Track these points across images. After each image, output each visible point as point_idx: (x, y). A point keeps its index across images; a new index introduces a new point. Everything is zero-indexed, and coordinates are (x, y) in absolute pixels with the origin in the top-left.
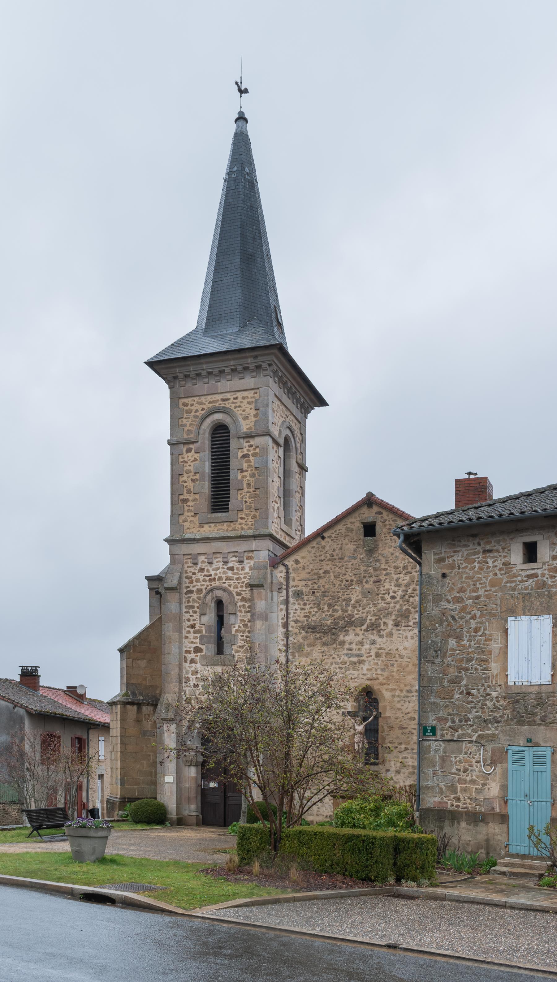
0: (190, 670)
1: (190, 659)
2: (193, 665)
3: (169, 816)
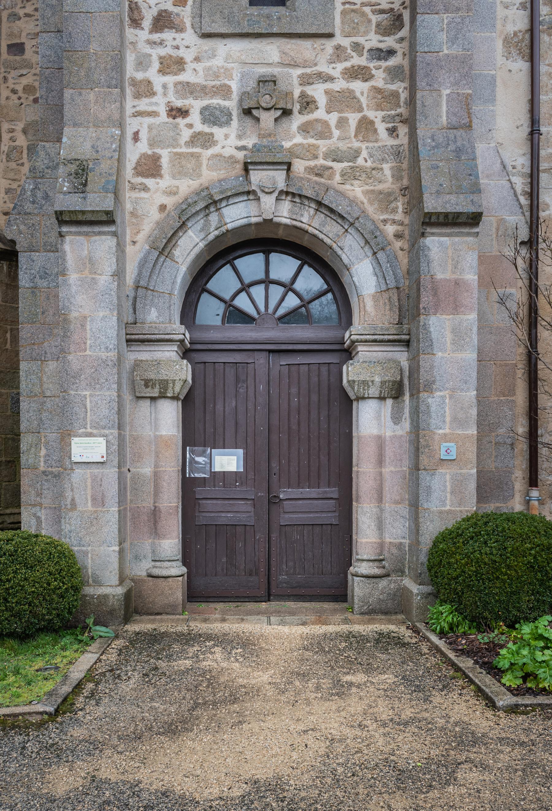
0: (156, 53)
1: (154, 12)
2: (168, 35)
3: (89, 590)
